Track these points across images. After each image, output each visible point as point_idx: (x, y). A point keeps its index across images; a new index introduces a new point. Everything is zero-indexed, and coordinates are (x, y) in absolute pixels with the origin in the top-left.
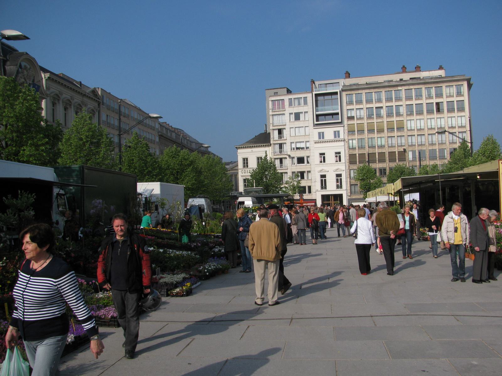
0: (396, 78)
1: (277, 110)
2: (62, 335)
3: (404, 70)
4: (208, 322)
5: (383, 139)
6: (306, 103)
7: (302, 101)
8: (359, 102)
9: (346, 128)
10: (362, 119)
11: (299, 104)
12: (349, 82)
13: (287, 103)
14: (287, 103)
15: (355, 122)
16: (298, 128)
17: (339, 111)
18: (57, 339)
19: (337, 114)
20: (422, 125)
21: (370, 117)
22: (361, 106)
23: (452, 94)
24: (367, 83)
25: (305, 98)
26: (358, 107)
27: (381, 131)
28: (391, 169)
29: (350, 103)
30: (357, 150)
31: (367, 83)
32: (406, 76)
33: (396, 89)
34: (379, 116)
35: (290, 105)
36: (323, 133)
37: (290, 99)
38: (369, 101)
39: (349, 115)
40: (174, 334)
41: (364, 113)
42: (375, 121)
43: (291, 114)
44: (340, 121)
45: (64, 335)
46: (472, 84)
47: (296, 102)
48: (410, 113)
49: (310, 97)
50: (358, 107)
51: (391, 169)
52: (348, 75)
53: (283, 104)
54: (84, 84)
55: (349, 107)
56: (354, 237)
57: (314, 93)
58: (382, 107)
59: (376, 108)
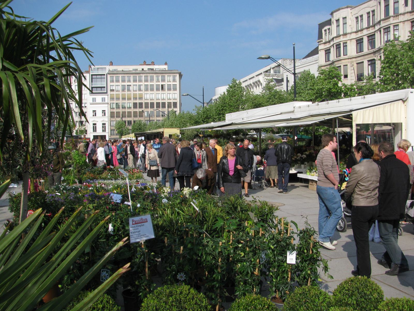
0: (140, 68)
3: (145, 63)
9: (109, 96)
12: (112, 68)
15: (115, 93)
17: (105, 86)
19: (105, 87)
21: (123, 90)
29: (112, 81)
32: (146, 68)
33: (139, 75)
34: (129, 90)
36: (95, 98)
38: (123, 81)
39: (111, 89)
41: (120, 88)
48: (147, 90)
52: (111, 64)
55: (112, 84)
59: (171, 82)
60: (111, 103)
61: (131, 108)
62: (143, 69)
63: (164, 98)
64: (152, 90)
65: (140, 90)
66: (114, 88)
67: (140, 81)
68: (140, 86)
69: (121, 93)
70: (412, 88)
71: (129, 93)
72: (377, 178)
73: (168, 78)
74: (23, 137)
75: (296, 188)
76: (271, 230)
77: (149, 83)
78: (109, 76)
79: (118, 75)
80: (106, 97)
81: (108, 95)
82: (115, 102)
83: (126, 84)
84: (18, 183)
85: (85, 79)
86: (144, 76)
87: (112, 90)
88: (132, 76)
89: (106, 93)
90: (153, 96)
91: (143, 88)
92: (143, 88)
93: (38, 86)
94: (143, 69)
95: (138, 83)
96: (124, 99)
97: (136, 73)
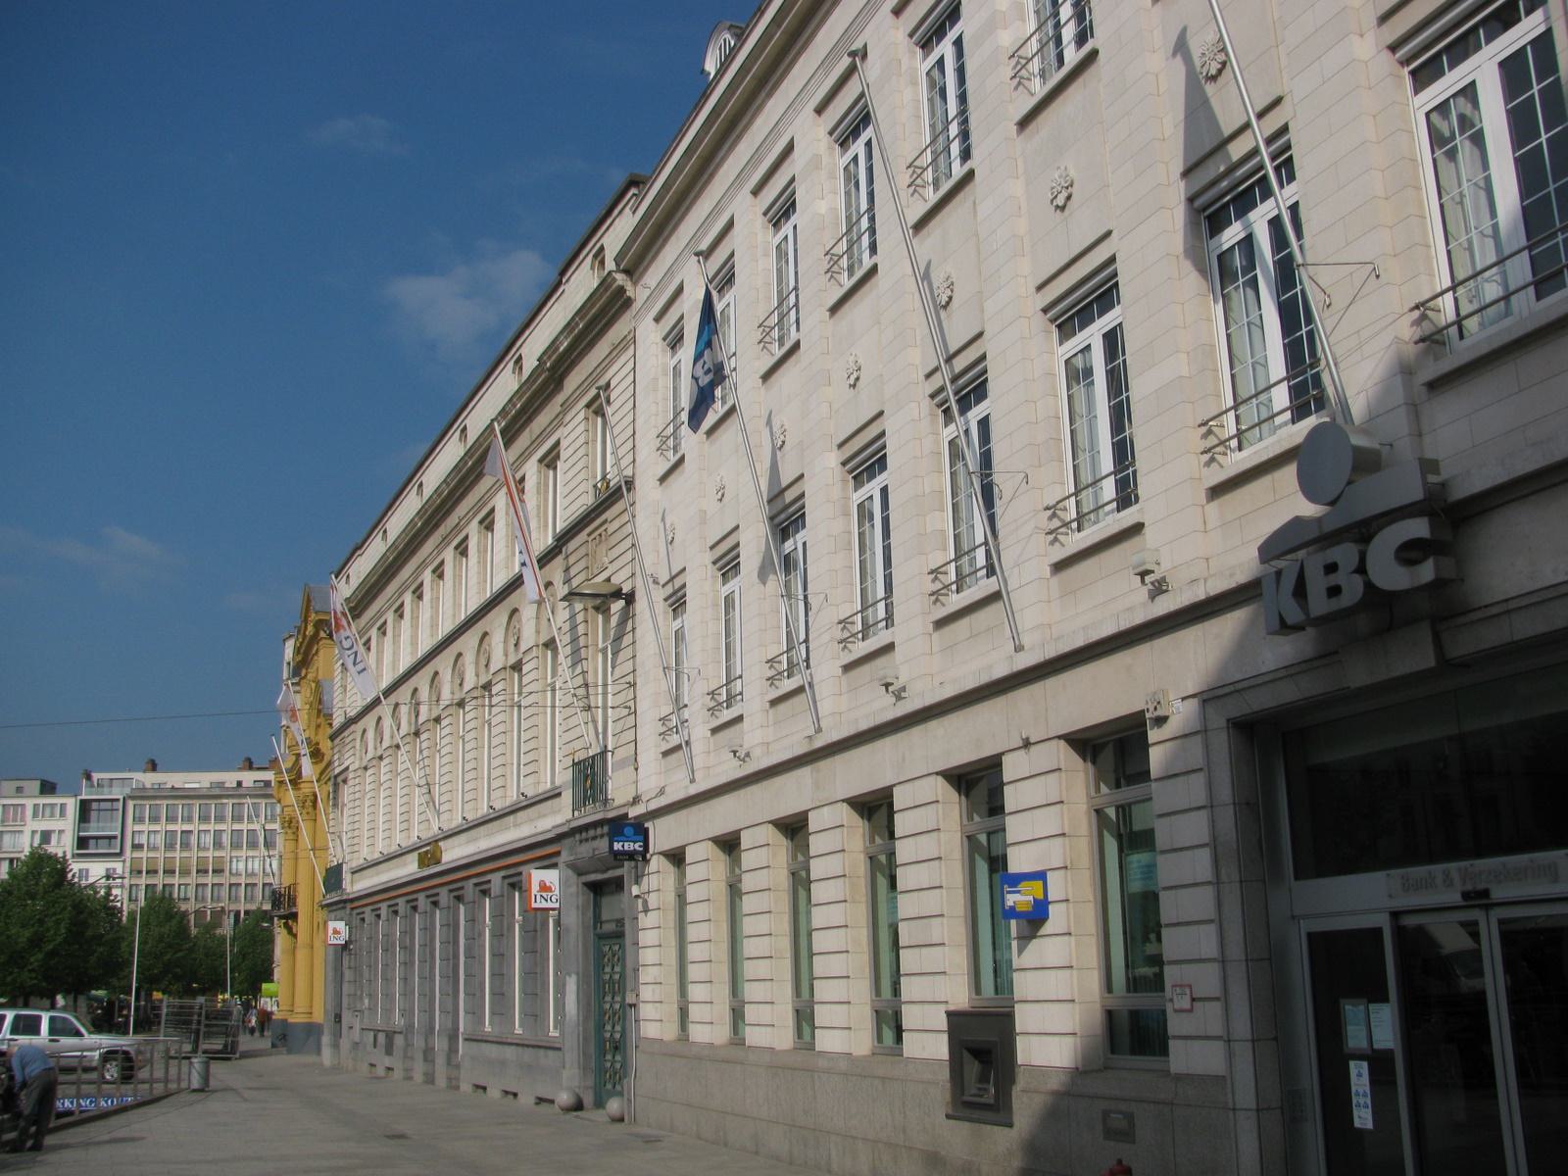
0: (230, 778)
1: (11, 823)
2: (1347, 437)
3: (250, 765)
5: (189, 888)
6: (63, 814)
7: (58, 810)
8: (155, 819)
9: (128, 864)
10: (155, 849)
11: (52, 815)
12: (149, 779)
13: (29, 812)
14: (29, 812)
15: (144, 854)
17: (118, 833)
18: (614, 286)
19: (115, 837)
20: (256, 866)
21: (169, 846)
22: (157, 828)
24: (173, 788)
25: (63, 806)
26: (153, 828)
27: (185, 872)
28: (247, 913)
29: (139, 820)
30: (1448, 197)
31: (173, 788)
32: (249, 778)
33: (219, 801)
34: (186, 846)
35: (35, 815)
36: (87, 870)
37: (36, 806)
38: (171, 819)
39: (136, 842)
41: (159, 840)
42: (177, 854)
43: (34, 832)
44: (118, 851)
45: (323, 1033)
46: (764, 584)
47: (48, 811)
48: (236, 845)
49: (72, 805)
50: (153, 828)
51: (247, 913)
52: (153, 767)
53: (23, 813)
55: (137, 828)
57: (79, 798)
58: (191, 832)
59: (182, 832)
60: (131, 886)
61: (189, 899)
62: (239, 784)
63: (256, 871)
64: (253, 845)
65: (218, 845)
67: (220, 819)
68: (218, 833)
69: (160, 855)
71: (185, 854)
74: (543, 376)
76: (77, 875)
77: (178, 827)
78: (131, 804)
79: (158, 802)
81: (124, 861)
82: (143, 881)
83: (178, 827)
84: (9, 873)
85: (347, 581)
86: (213, 806)
87: (137, 847)
88: (197, 803)
89: (121, 853)
90: (256, 866)
91: (226, 839)
92: (226, 839)
93: (597, 919)
94: (239, 784)
95: (212, 827)
96: (169, 872)
97: (217, 793)
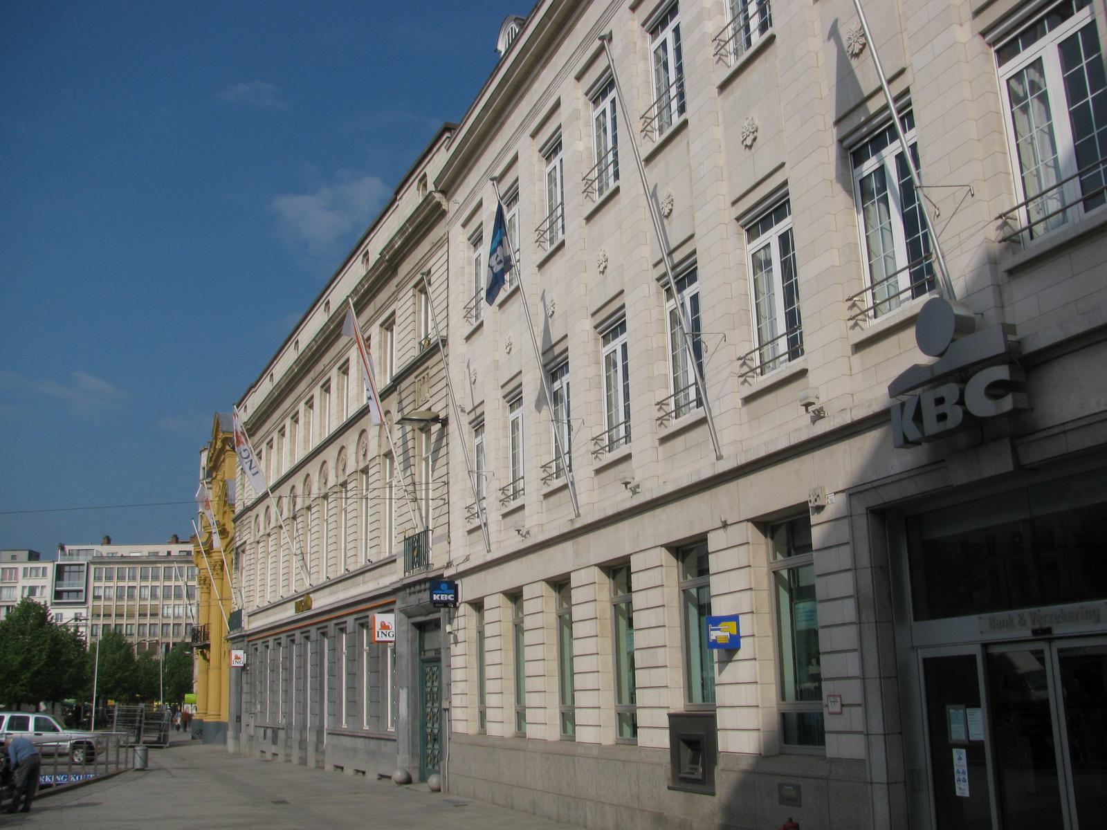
0: (162, 549)
1: (8, 581)
3: (176, 540)
4: (890, 229)
5: (134, 626)
6: (44, 574)
7: (41, 572)
8: (109, 578)
9: (90, 610)
12: (105, 550)
13: (21, 573)
14: (21, 573)
15: (101, 603)
16: (76, 593)
17: (83, 588)
19: (81, 591)
21: (120, 597)
22: (111, 584)
23: (146, 597)
24: (122, 556)
25: (44, 569)
26: (108, 584)
28: (174, 644)
29: (98, 579)
31: (122, 556)
32: (176, 549)
33: (155, 566)
34: (131, 597)
35: (25, 575)
36: (62, 614)
37: (25, 569)
38: (121, 578)
39: (96, 594)
40: (367, 598)
41: (113, 593)
42: (125, 603)
43: (24, 587)
44: (83, 601)
48: (167, 597)
51: (174, 644)
52: (108, 541)
53: (16, 574)
54: (345, 434)
55: (97, 584)
56: (22, 811)
58: (135, 587)
59: (129, 587)
60: (92, 625)
61: (133, 635)
64: (178, 596)
65: (154, 596)
66: (101, 593)
67: (155, 578)
68: (154, 588)
69: (113, 603)
70: (204, 742)
71: (131, 603)
72: (963, 304)
73: (131, 571)
75: (919, 429)
77: (126, 584)
78: (92, 567)
79: (112, 566)
80: (83, 612)
81: (87, 608)
83: (126, 584)
87: (97, 598)
88: (139, 566)
89: (85, 602)
90: (181, 611)
91: (159, 592)
92: (159, 592)
94: (169, 553)
95: (149, 583)
96: (119, 615)
97: (154, 560)
